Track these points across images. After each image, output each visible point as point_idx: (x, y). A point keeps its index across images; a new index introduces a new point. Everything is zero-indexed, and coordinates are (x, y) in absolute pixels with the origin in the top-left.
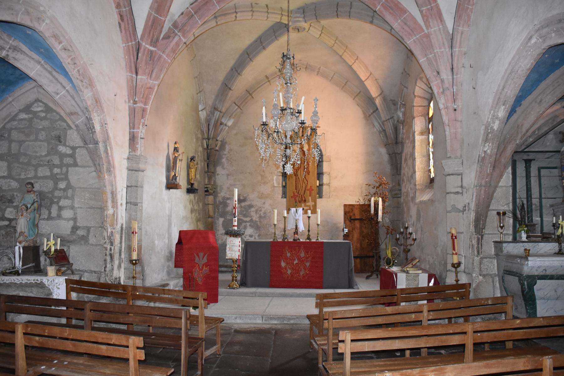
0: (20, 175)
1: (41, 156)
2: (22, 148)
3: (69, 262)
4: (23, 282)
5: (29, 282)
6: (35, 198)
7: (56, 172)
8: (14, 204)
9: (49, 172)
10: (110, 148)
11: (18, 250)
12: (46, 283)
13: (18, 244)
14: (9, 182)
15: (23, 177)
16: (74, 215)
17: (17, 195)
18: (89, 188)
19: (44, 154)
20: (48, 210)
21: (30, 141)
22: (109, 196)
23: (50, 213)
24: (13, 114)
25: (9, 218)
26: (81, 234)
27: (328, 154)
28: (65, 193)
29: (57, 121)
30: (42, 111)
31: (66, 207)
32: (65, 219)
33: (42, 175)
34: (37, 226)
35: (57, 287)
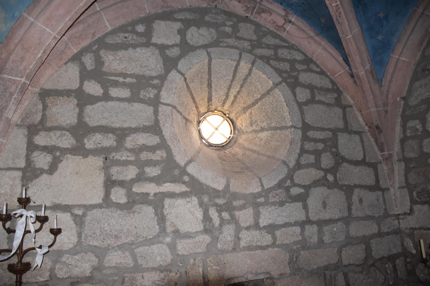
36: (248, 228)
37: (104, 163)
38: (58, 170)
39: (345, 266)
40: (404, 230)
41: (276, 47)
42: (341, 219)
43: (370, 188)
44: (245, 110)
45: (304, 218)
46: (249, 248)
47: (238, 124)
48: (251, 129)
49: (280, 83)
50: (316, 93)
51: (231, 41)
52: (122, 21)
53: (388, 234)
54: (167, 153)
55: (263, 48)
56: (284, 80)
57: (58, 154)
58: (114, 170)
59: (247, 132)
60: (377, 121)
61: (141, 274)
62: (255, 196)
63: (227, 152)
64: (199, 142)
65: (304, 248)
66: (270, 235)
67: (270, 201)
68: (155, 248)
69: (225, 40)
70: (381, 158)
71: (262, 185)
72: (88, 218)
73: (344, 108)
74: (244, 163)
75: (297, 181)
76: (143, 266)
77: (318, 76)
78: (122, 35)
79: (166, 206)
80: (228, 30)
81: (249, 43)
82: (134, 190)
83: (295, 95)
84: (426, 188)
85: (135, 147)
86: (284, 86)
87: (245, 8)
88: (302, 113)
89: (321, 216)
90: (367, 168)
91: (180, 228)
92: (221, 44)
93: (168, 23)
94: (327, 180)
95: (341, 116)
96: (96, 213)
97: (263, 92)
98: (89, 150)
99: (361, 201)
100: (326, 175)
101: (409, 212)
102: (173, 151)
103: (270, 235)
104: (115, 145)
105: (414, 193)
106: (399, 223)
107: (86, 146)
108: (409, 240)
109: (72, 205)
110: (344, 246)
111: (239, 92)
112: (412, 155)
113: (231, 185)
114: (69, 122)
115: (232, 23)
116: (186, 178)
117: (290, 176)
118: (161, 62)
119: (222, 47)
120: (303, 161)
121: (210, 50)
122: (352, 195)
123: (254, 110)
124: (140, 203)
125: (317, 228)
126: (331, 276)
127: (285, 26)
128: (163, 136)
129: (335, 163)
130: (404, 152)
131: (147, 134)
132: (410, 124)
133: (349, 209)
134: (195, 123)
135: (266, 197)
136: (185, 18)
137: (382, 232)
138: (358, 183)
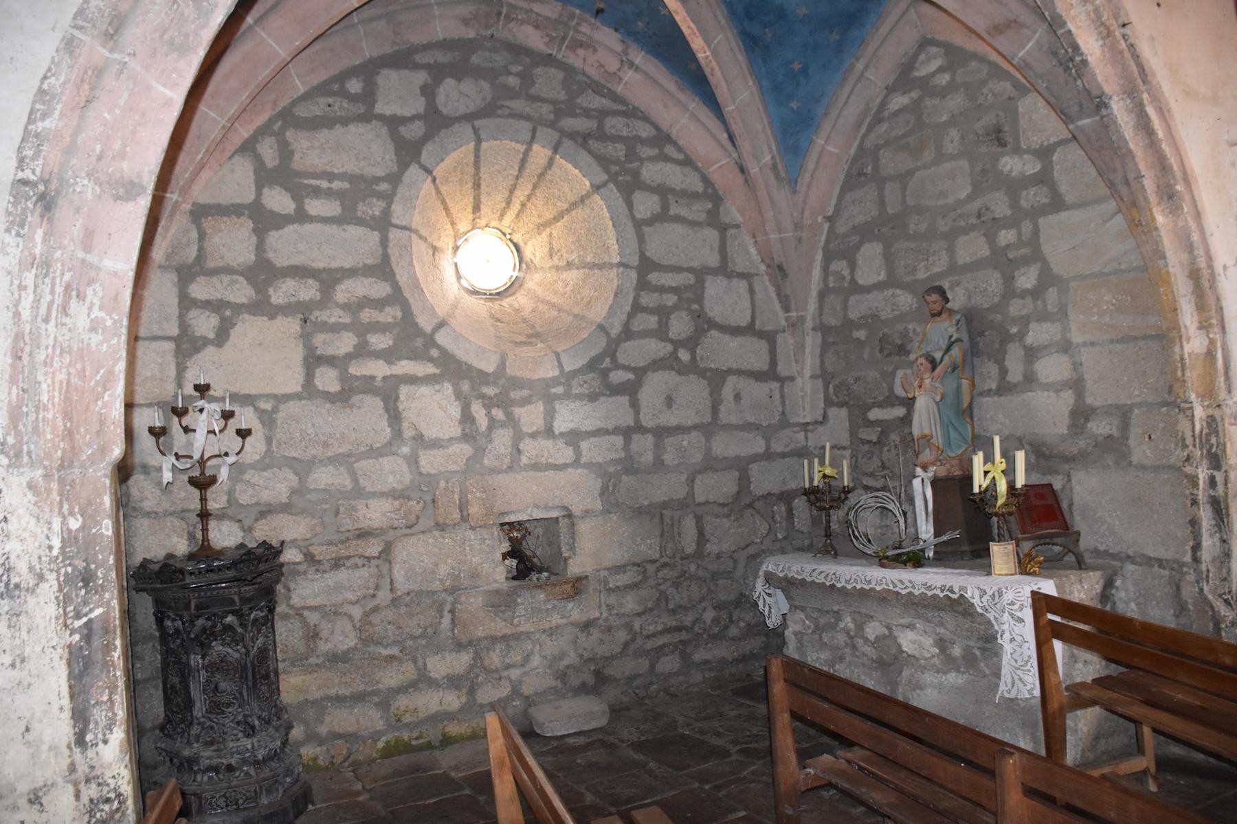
0: (914, 270)
1: (960, 203)
2: (907, 193)
3: (1065, 527)
5: (930, 593)
6: (952, 330)
9: (986, 247)
10: (1160, 111)
11: (922, 490)
12: (976, 601)
13: (919, 470)
16: (1075, 369)
17: (914, 330)
18: (1109, 274)
19: (963, 194)
20: (996, 362)
21: (925, 167)
22: (1182, 287)
23: (1004, 372)
24: (874, 107)
26: (1100, 431)
28: (1039, 302)
29: (984, 83)
30: (941, 70)
31: (1046, 347)
33: (968, 260)
34: (969, 412)
35: (1012, 616)
36: (533, 435)
37: (302, 327)
38: (231, 338)
39: (699, 504)
41: (602, 114)
43: (759, 376)
44: (541, 227)
45: (630, 421)
46: (536, 467)
47: (528, 252)
48: (550, 263)
49: (604, 185)
50: (671, 202)
51: (517, 105)
52: (323, 75)
53: (783, 455)
54: (403, 310)
55: (575, 116)
56: (613, 178)
57: (228, 313)
58: (319, 339)
59: (542, 268)
61: (364, 501)
62: (548, 383)
63: (504, 304)
64: (456, 286)
65: (627, 471)
66: (571, 448)
67: (574, 392)
68: (386, 463)
69: (507, 103)
70: (784, 323)
71: (560, 366)
72: (281, 415)
73: (723, 229)
74: (533, 327)
75: (622, 359)
76: (367, 489)
77: (678, 168)
78: (323, 101)
79: (402, 397)
80: (513, 81)
81: (551, 108)
82: (352, 370)
83: (630, 206)
85: (351, 301)
86: (612, 190)
87: (547, 39)
88: (641, 239)
90: (755, 339)
91: (424, 432)
92: (499, 112)
93: (404, 73)
94: (677, 358)
95: (716, 244)
96: (293, 407)
97: (572, 199)
98: (276, 306)
99: (738, 397)
101: (820, 419)
102: (413, 308)
103: (571, 448)
104: (318, 298)
106: (806, 438)
107: (273, 300)
109: (255, 396)
110: (700, 472)
111: (529, 197)
112: (833, 322)
113: (507, 364)
114: (241, 260)
115: (520, 68)
116: (434, 353)
117: (611, 351)
118: (392, 150)
119: (499, 116)
120: (636, 326)
121: (477, 123)
122: (722, 386)
123: (557, 230)
124: (360, 393)
126: (672, 518)
127: (621, 74)
128: (397, 283)
129: (696, 330)
131: (370, 280)
133: (715, 410)
134: (450, 251)
135: (568, 385)
136: (435, 62)
138: (735, 366)
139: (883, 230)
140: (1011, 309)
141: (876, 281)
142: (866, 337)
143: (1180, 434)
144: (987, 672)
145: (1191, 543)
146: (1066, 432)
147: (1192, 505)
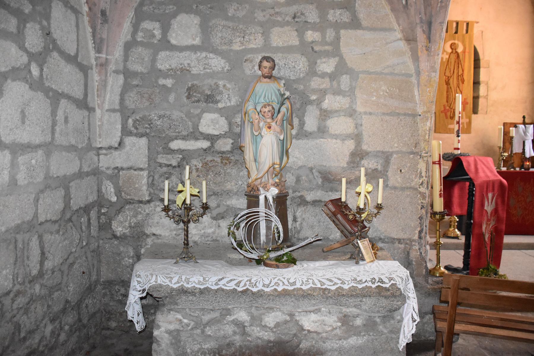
0: (231, 42)
4: (346, 287)
5: (360, 286)
7: (310, 39)
8: (220, 105)
14: (206, 57)
15: (238, 48)
18: (386, 74)
23: (302, 124)
25: (208, 135)
27: (486, 58)
31: (336, 111)
32: (336, 137)
33: (281, 44)
40: (105, 170)
42: (42, 145)
60: (106, 3)
70: (94, 62)
84: (150, 115)
89: (18, 136)
100: (29, 64)
101: (116, 146)
105: (130, 121)
108: (110, 184)
110: (42, 191)
112: (138, 68)
125: (10, 158)
130: (126, 62)
132: (147, 25)
137: (82, 171)
139: (201, 7)
140: (312, 83)
141: (190, 44)
142: (173, 85)
143: (419, 170)
144: (385, 331)
145: (419, 229)
146: (345, 166)
147: (421, 208)
